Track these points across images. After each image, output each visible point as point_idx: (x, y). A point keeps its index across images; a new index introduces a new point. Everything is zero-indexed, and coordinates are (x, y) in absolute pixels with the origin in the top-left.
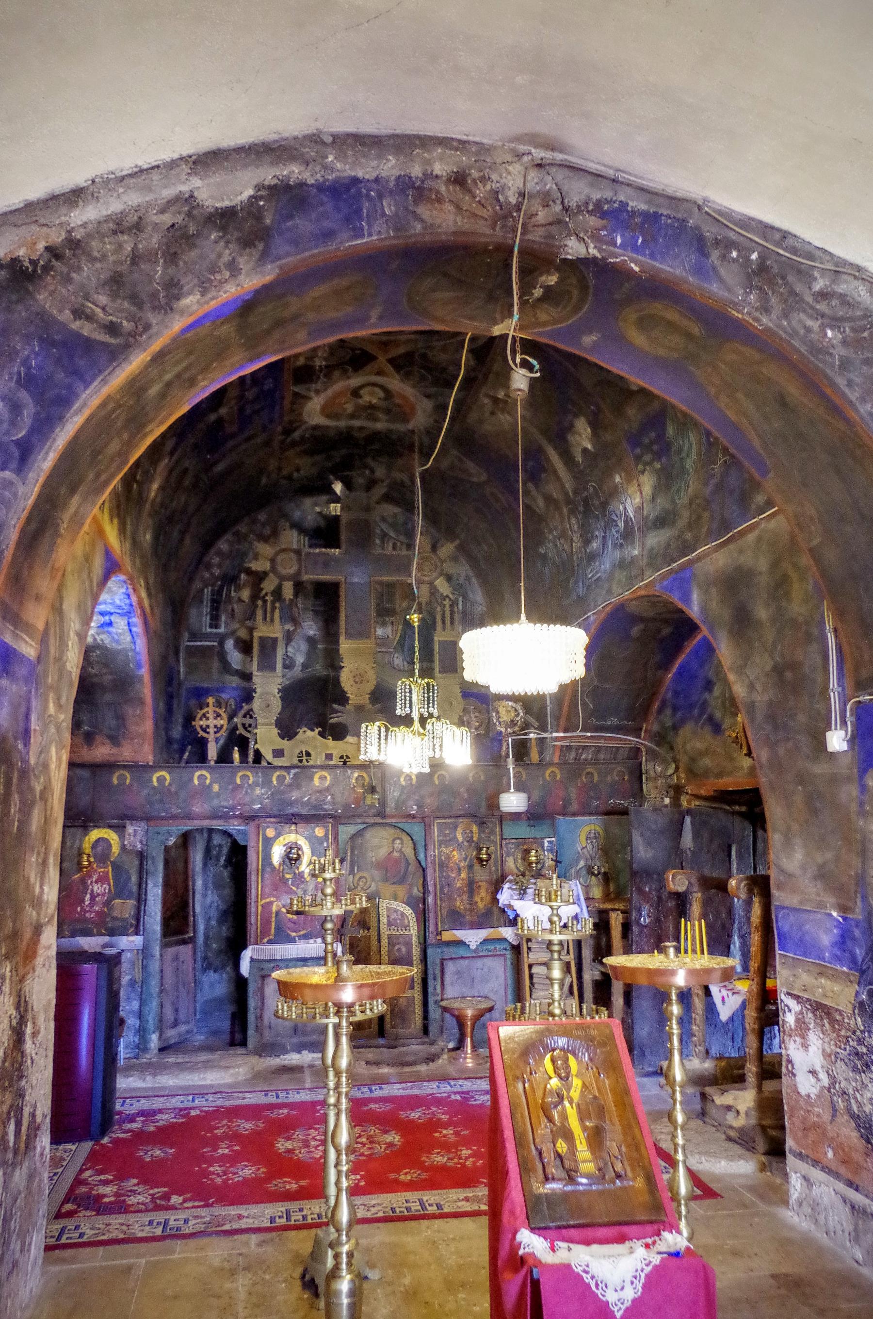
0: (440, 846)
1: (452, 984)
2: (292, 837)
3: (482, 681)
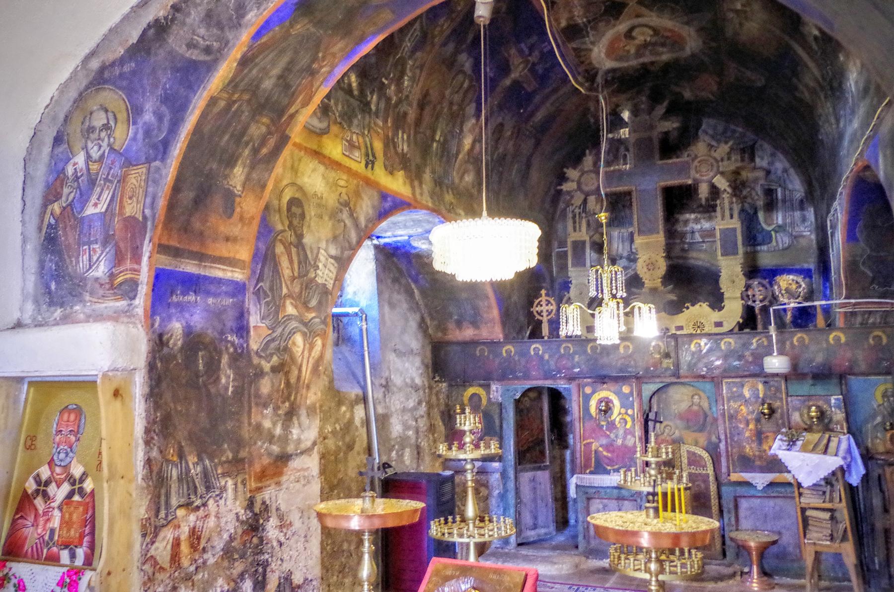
0: (729, 401)
1: (746, 517)
2: (603, 394)
3: (449, 271)
